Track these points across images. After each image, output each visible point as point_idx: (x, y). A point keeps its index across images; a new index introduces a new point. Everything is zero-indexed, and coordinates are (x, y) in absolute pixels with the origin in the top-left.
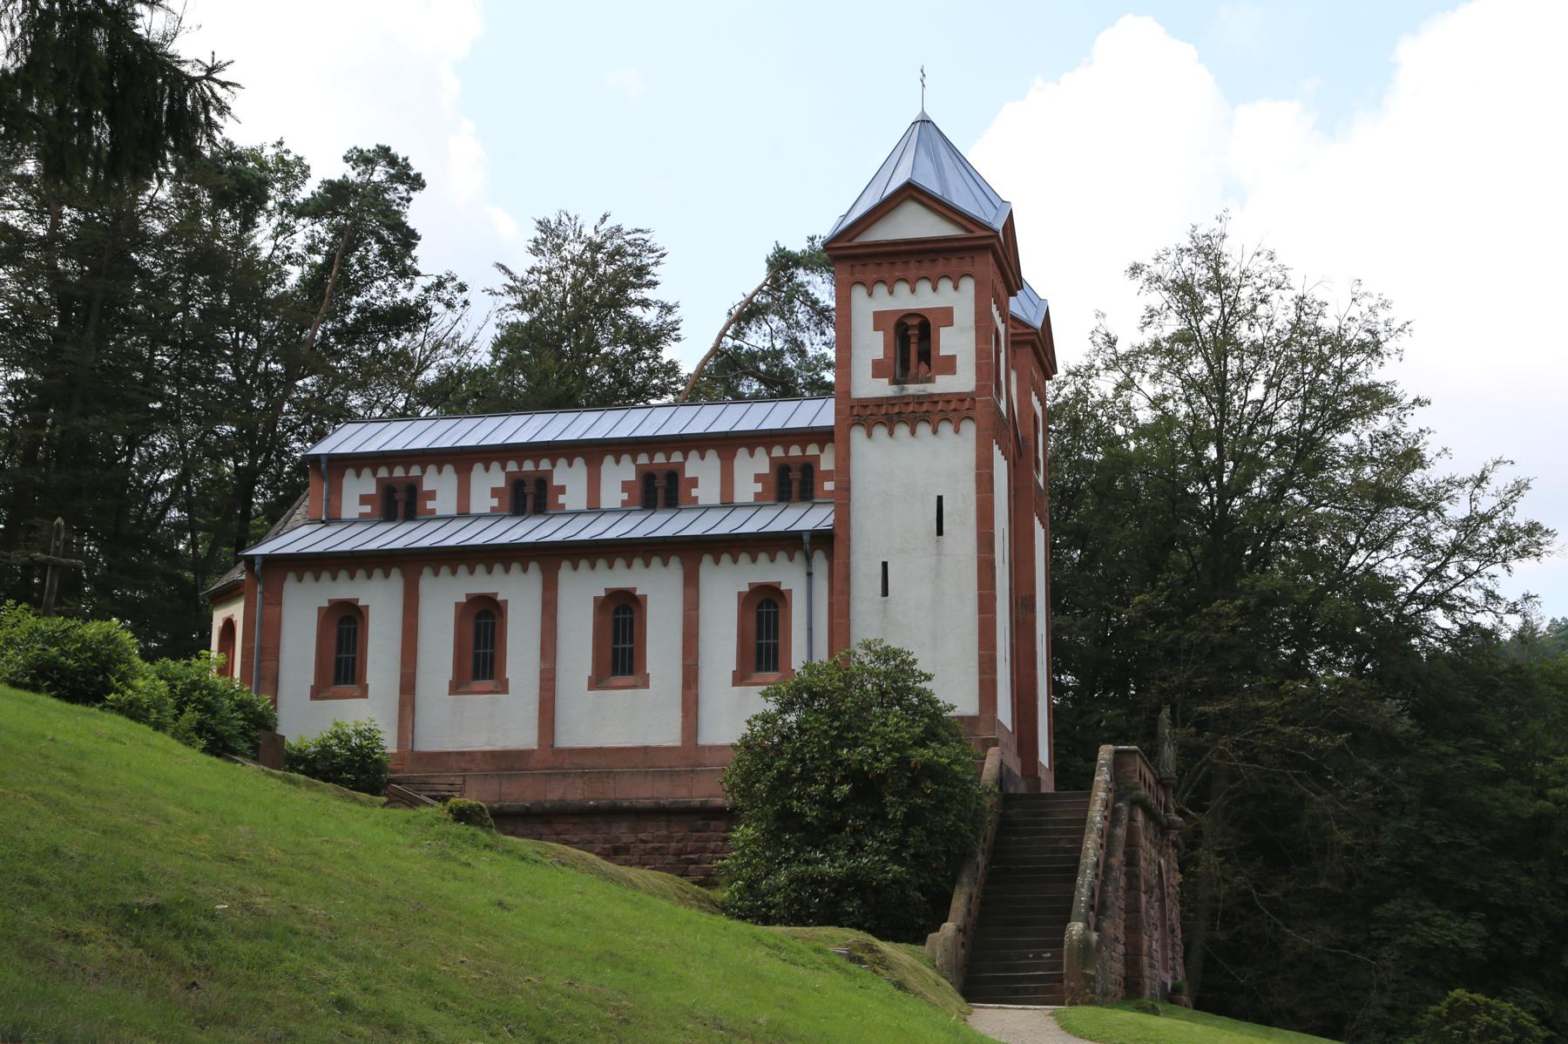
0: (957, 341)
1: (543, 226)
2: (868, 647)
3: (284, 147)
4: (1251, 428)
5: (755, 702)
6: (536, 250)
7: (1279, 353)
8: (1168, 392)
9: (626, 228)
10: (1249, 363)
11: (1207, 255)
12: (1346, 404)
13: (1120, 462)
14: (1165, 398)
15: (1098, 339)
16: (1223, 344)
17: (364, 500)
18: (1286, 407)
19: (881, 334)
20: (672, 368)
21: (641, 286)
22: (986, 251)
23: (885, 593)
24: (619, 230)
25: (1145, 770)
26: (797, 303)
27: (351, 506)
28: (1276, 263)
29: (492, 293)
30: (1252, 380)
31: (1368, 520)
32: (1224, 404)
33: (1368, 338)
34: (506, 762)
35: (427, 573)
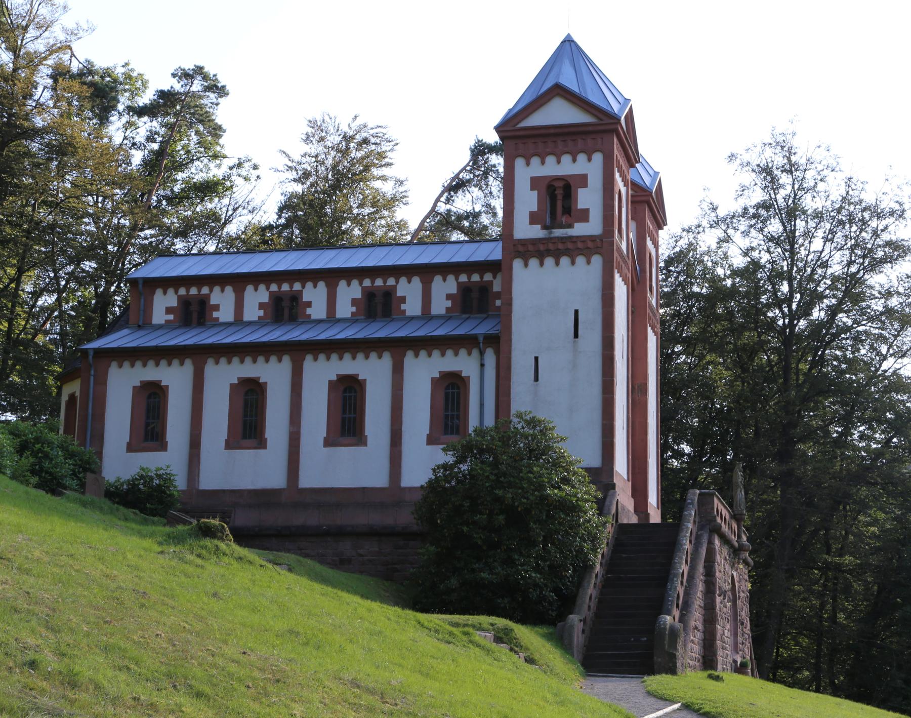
0: (588, 198)
1: (312, 123)
2: (519, 415)
3: (130, 67)
4: (813, 270)
5: (440, 456)
6: (308, 139)
7: (833, 218)
8: (754, 245)
9: (370, 125)
10: (812, 224)
11: (782, 147)
12: (880, 254)
13: (719, 293)
14: (752, 249)
15: (705, 206)
16: (792, 212)
17: (169, 310)
18: (837, 256)
19: (536, 192)
20: (402, 225)
21: (381, 166)
22: (607, 131)
23: (536, 379)
24: (365, 126)
25: (721, 507)
26: (491, 179)
27: (159, 316)
28: (831, 153)
29: (277, 170)
30: (813, 237)
31: (896, 337)
32: (793, 253)
33: (897, 207)
34: (262, 498)
35: (210, 362)
